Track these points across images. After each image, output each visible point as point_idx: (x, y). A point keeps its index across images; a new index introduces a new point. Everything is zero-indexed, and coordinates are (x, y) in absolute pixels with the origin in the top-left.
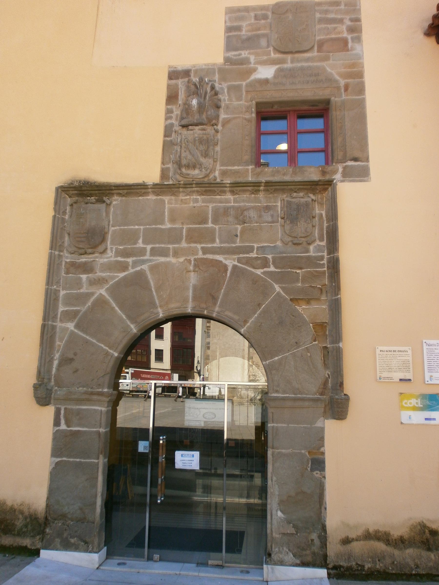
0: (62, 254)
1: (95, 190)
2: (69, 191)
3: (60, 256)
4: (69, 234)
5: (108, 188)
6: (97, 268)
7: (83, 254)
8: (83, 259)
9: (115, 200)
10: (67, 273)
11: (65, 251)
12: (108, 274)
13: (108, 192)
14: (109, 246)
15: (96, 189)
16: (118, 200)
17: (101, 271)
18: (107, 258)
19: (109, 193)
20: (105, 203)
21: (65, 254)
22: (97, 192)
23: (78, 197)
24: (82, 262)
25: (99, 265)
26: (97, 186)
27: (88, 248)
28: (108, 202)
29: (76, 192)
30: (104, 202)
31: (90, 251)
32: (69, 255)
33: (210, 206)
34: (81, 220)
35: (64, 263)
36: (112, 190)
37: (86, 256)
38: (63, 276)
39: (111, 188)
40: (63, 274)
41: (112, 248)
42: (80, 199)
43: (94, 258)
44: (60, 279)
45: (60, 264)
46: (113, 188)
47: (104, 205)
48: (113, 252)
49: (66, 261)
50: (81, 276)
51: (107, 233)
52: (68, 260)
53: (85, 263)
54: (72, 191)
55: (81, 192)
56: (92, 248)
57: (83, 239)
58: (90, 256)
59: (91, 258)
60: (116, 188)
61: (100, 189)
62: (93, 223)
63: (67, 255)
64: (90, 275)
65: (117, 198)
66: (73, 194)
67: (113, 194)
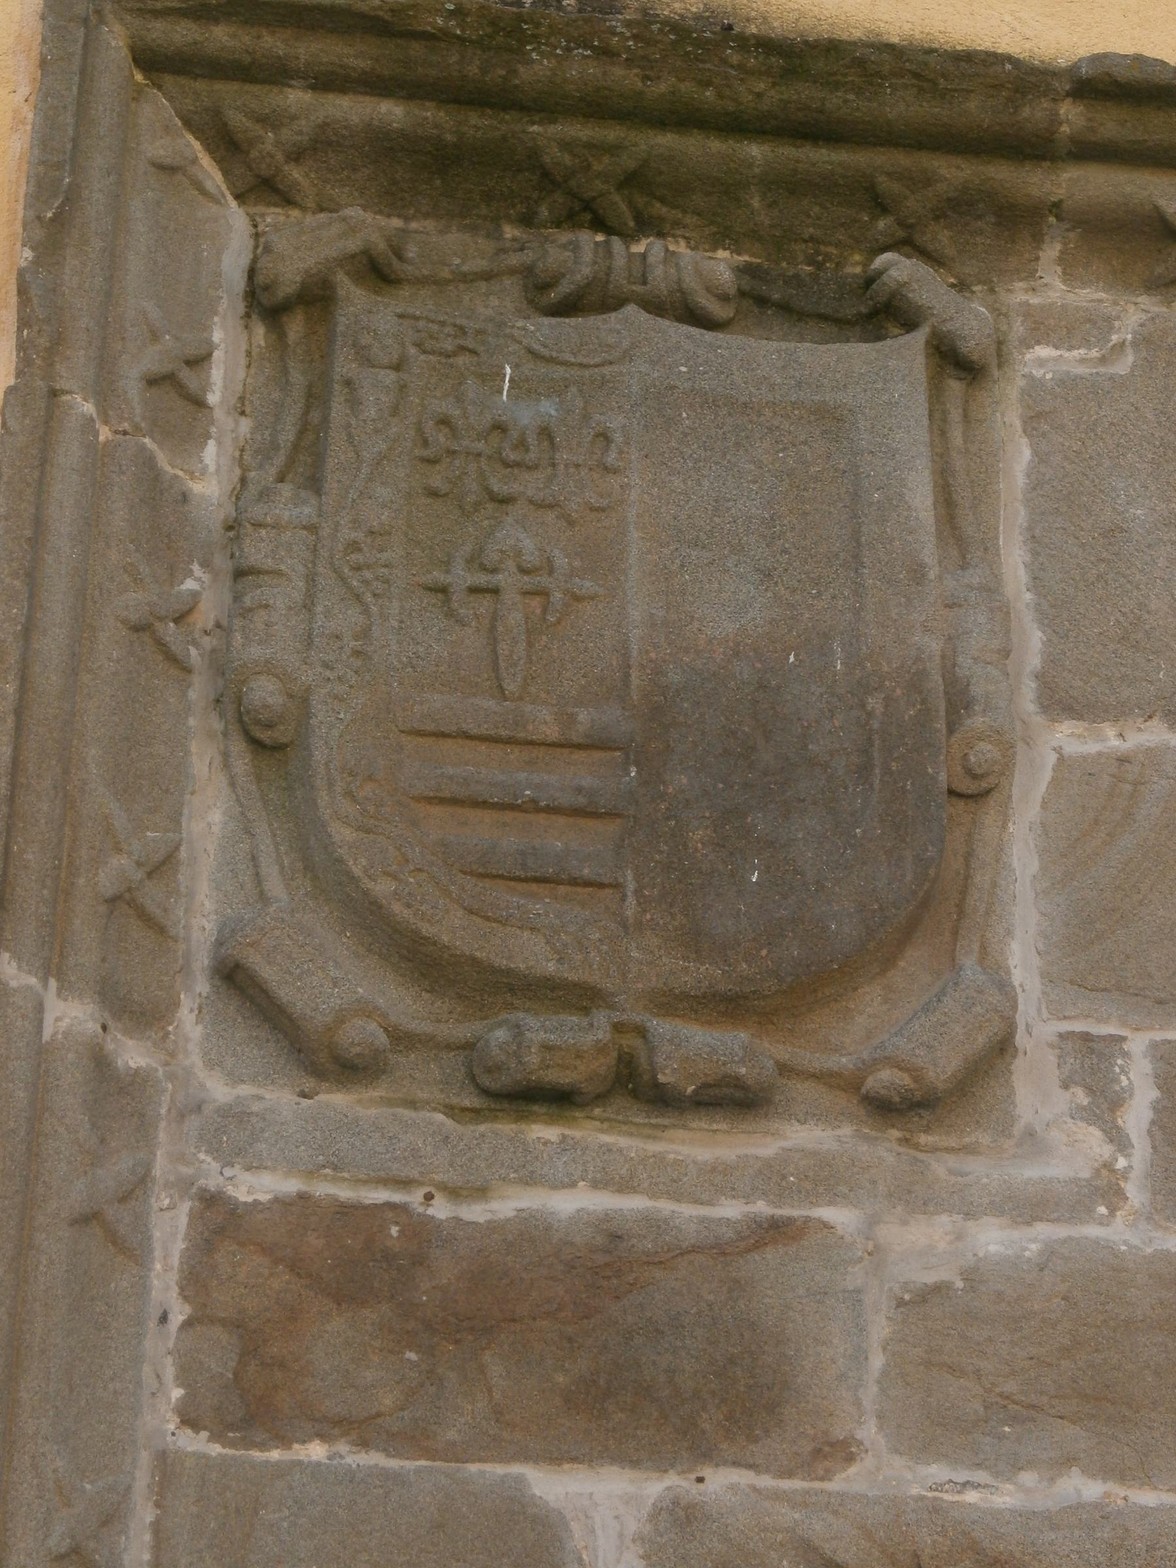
0: (133, 1055)
1: (737, 125)
2: (277, 74)
3: (117, 1097)
4: (268, 745)
5: (976, 110)
6: (857, 1367)
7: (559, 1100)
8: (565, 1187)
9: (1042, 327)
10: (252, 1398)
11: (189, 1023)
12: (1092, 1490)
13: (953, 172)
14: (1039, 1028)
15: (759, 93)
16: (1108, 324)
17: (933, 1430)
18: (1028, 1207)
19: (959, 207)
20: (918, 339)
21: (197, 1056)
22: (756, 151)
23: (391, 199)
24: (529, 1233)
25: (880, 1328)
26: (768, 45)
27: (671, 1002)
28: (970, 320)
29: (391, 112)
30: (885, 315)
31: (690, 1047)
32: (280, 1099)
33: (1138, 1044)
34: (518, 537)
35: (170, 1229)
36: (1035, 149)
37: (592, 1134)
38: (167, 1465)
39: (1034, 113)
40: (161, 1416)
41: (1090, 1060)
42: (438, 242)
43: (772, 1177)
44: (112, 1517)
45: (109, 1228)
46: (1072, 116)
47: (907, 353)
48: (1137, 1117)
49: (211, 1200)
50: (551, 1486)
51: (977, 792)
52: (254, 1187)
53: (607, 1265)
54: (327, 82)
55: (479, 125)
56: (726, 1006)
57: (557, 839)
58: (697, 1145)
59: (720, 1180)
60: (1112, 124)
61: (842, 103)
62: (731, 611)
63: (220, 1091)
64: (721, 1483)
65: (1089, 296)
66: (321, 145)
67: (1020, 221)
